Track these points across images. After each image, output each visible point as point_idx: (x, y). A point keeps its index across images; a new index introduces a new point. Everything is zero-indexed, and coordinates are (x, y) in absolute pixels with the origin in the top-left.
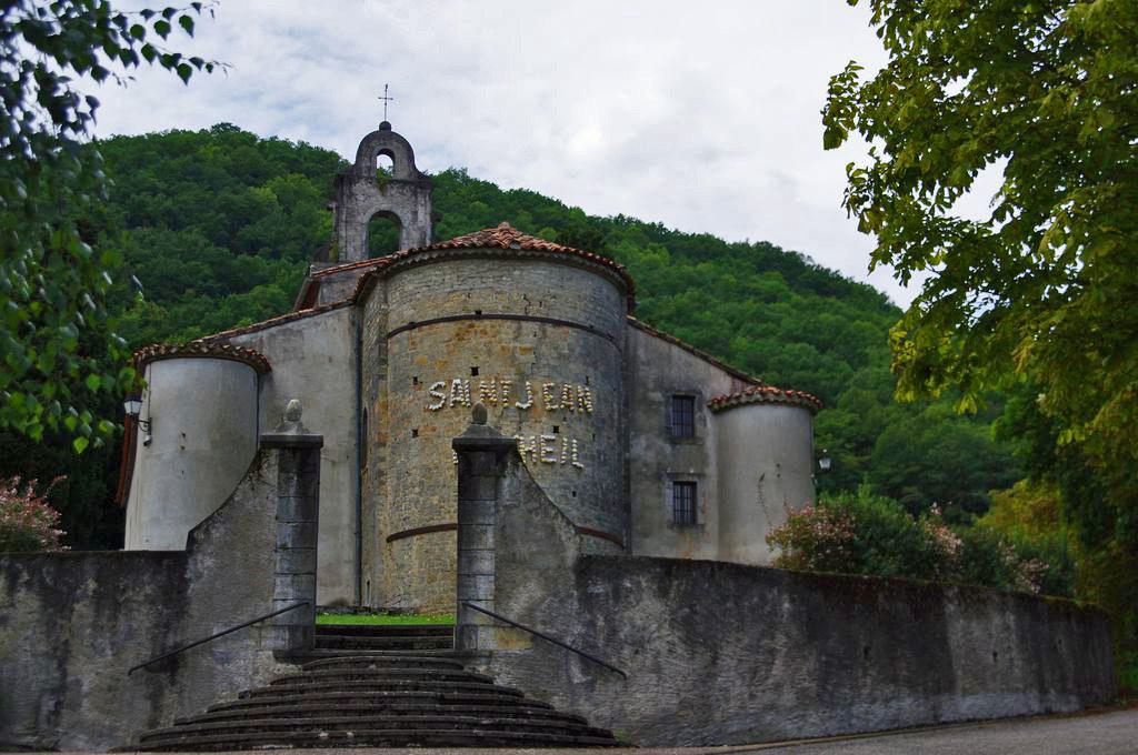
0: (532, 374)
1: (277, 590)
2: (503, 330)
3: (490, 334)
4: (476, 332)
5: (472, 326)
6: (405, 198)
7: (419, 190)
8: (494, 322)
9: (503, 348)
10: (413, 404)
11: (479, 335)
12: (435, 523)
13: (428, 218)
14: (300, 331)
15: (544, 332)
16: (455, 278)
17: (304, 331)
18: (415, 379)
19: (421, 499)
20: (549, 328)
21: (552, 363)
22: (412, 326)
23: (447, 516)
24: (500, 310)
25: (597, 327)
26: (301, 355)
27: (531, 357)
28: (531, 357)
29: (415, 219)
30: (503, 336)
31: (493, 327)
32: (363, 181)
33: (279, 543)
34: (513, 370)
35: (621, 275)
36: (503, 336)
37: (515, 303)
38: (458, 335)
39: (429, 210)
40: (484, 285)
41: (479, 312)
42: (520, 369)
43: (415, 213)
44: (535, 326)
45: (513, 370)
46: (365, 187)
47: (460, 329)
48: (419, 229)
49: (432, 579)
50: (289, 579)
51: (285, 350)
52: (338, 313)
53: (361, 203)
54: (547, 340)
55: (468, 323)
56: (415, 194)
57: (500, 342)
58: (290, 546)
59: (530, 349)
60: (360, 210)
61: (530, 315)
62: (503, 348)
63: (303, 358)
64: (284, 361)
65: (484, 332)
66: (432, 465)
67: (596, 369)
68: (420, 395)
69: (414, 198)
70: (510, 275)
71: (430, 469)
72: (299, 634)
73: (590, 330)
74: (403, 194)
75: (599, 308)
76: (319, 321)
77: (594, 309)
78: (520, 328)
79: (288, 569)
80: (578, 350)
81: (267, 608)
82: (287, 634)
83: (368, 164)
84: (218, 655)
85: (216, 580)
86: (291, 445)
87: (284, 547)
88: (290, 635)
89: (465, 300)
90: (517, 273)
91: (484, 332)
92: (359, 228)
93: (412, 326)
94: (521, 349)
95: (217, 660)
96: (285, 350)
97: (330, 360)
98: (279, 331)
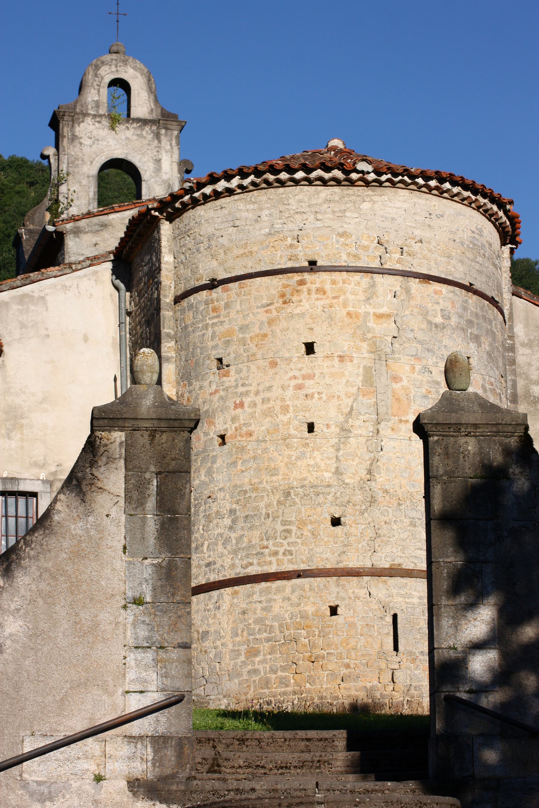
0: (393, 352)
1: (131, 675)
2: (349, 287)
3: (329, 294)
4: (309, 291)
5: (302, 283)
6: (145, 142)
7: (163, 131)
8: (336, 276)
9: (349, 314)
10: (217, 396)
11: (314, 296)
12: (253, 570)
13: (175, 167)
14: (42, 298)
15: (408, 291)
16: (275, 212)
17: (48, 298)
18: (220, 360)
19: (233, 535)
20: (414, 283)
21: (420, 336)
22: (213, 284)
23: (273, 559)
24: (343, 260)
25: (477, 286)
26: (43, 332)
27: (390, 327)
28: (390, 327)
29: (158, 170)
30: (351, 297)
31: (334, 282)
32: (89, 120)
33: (130, 594)
34: (365, 345)
35: (506, 212)
36: (351, 297)
37: (366, 248)
38: (283, 295)
39: (176, 157)
40: (319, 224)
41: (313, 263)
42: (375, 343)
43: (158, 161)
44: (395, 282)
45: (365, 345)
46: (91, 127)
47: (285, 286)
48: (164, 182)
49: (253, 653)
50: (150, 655)
51: (23, 326)
52: (96, 272)
53: (86, 150)
54: (412, 302)
55: (297, 277)
56: (157, 136)
57: (345, 305)
58: (148, 599)
59: (388, 316)
60: (86, 158)
61: (386, 266)
62: (349, 314)
63: (48, 336)
64: (20, 340)
65: (321, 291)
66: (248, 487)
67: (479, 345)
68: (227, 384)
69: (156, 142)
70: (358, 209)
71: (245, 492)
72: (170, 753)
73: (469, 288)
74: (140, 136)
75: (480, 259)
76: (68, 284)
77: (474, 260)
78: (373, 285)
79: (148, 639)
80: (454, 320)
81: (114, 706)
82: (149, 750)
83: (96, 98)
84: (33, 786)
85: (25, 657)
86: (116, 429)
87: (138, 602)
88: (155, 752)
89: (291, 246)
90: (366, 206)
91: (321, 291)
92: (84, 182)
93: (213, 284)
94: (375, 314)
95: (32, 794)
96: (23, 326)
97: (86, 339)
98: (13, 298)
